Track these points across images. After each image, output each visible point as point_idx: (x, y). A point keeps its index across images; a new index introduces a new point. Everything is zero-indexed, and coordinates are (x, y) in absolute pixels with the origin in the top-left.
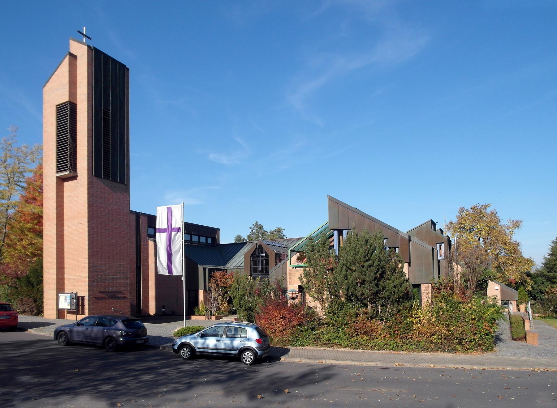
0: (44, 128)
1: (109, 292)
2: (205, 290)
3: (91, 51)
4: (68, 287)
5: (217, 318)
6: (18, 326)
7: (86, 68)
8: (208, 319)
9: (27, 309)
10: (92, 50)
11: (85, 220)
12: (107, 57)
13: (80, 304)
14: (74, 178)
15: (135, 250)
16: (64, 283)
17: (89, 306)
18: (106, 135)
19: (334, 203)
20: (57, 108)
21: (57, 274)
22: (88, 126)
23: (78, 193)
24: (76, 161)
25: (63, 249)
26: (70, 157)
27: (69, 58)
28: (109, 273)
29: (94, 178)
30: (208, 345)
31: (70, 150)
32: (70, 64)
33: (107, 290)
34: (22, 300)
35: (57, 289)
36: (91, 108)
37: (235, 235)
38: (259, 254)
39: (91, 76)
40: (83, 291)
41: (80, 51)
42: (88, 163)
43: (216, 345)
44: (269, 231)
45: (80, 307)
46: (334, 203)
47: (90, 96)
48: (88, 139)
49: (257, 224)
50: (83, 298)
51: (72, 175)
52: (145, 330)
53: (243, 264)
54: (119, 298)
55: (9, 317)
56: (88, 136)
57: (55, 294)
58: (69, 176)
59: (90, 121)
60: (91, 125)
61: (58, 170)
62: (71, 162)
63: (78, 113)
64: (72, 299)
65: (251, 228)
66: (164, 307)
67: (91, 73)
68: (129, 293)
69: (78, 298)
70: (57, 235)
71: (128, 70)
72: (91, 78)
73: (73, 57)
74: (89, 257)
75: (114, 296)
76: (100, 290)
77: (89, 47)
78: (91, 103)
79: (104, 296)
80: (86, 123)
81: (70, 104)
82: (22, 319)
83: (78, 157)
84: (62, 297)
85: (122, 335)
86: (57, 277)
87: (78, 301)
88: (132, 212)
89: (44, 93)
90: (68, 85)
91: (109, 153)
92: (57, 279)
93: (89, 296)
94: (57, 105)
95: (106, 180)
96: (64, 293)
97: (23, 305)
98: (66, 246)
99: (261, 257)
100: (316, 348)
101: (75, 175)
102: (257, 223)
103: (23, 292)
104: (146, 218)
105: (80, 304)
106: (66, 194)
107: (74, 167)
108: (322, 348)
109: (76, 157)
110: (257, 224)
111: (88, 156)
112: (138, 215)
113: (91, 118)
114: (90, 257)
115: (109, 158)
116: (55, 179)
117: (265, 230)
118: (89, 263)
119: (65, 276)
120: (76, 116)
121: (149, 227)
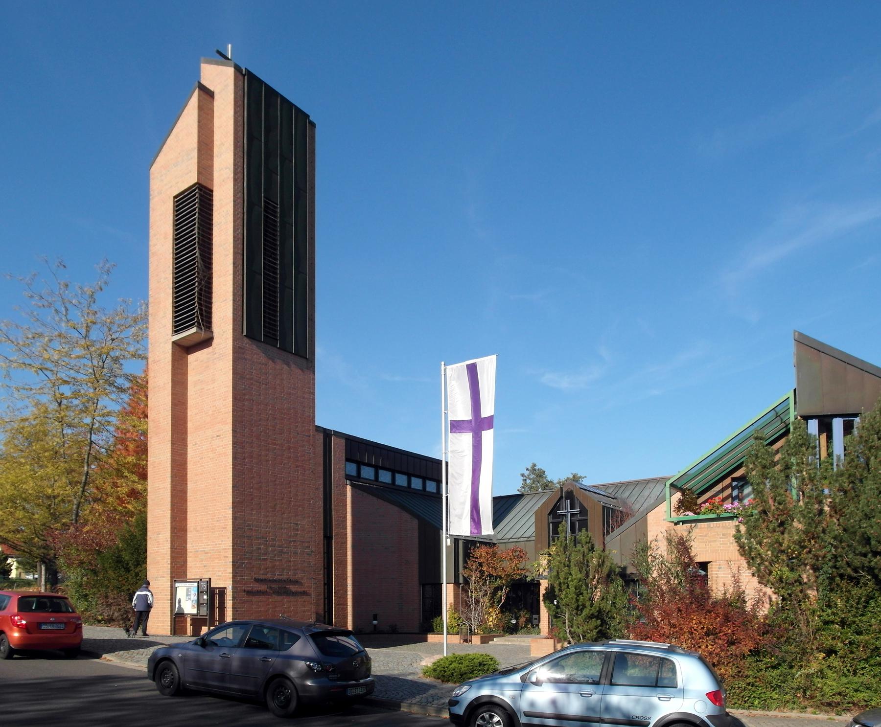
0: (151, 248)
1: (274, 581)
2: (456, 583)
3: (241, 77)
4: (194, 569)
5: (484, 640)
6: (83, 648)
7: (232, 113)
8: (466, 641)
9: (116, 614)
10: (244, 76)
11: (228, 428)
12: (271, 93)
13: (217, 605)
14: (207, 342)
15: (321, 503)
16: (185, 562)
17: (234, 608)
18: (270, 254)
19: (808, 346)
20: (174, 202)
21: (172, 543)
22: (234, 231)
23: (214, 373)
24: (211, 308)
25: (185, 492)
26: (199, 299)
27: (199, 96)
28: (274, 540)
29: (246, 340)
30: (532, 704)
31: (200, 284)
32: (200, 108)
33: (269, 576)
34: (107, 597)
35: (172, 572)
36: (240, 195)
37: (523, 467)
38: (566, 509)
39: (241, 128)
40: (223, 579)
41: (221, 79)
42: (234, 310)
43: (554, 703)
44: (555, 481)
45: (217, 611)
46: (808, 346)
47: (240, 169)
48: (234, 259)
49: (533, 469)
50: (222, 591)
51: (203, 335)
52: (366, 661)
53: (533, 529)
54: (295, 594)
55: (62, 627)
56: (235, 253)
57: (169, 584)
58: (197, 339)
59: (239, 221)
60: (240, 230)
61: (177, 329)
62: (201, 309)
63: (215, 208)
64: (200, 593)
65: (523, 475)
66: (375, 618)
67: (241, 123)
68: (312, 584)
69: (211, 592)
70: (173, 461)
71: (313, 125)
72: (240, 133)
73: (207, 94)
74: (236, 505)
75: (282, 588)
76: (257, 576)
77: (237, 69)
78: (240, 184)
79: (263, 587)
80: (231, 225)
81: (200, 190)
82: (91, 632)
83: (214, 300)
84: (182, 590)
85: (310, 673)
86: (173, 548)
87: (212, 596)
88: (319, 429)
89: (152, 177)
90: (196, 151)
91: (276, 292)
92: (172, 552)
93: (234, 587)
94: (175, 197)
95: (269, 347)
96: (186, 582)
97: (109, 605)
98: (190, 486)
99: (572, 515)
100: (803, 715)
101: (208, 335)
102: (534, 465)
103: (109, 580)
104: (343, 441)
105: (217, 605)
106: (192, 378)
107: (206, 320)
108: (822, 716)
109: (211, 298)
110: (533, 469)
111: (234, 295)
112: (327, 434)
113: (240, 215)
114: (238, 505)
115: (275, 321)
116: (169, 348)
117: (549, 479)
118: (234, 519)
119: (189, 546)
120: (211, 215)
121: (348, 460)
